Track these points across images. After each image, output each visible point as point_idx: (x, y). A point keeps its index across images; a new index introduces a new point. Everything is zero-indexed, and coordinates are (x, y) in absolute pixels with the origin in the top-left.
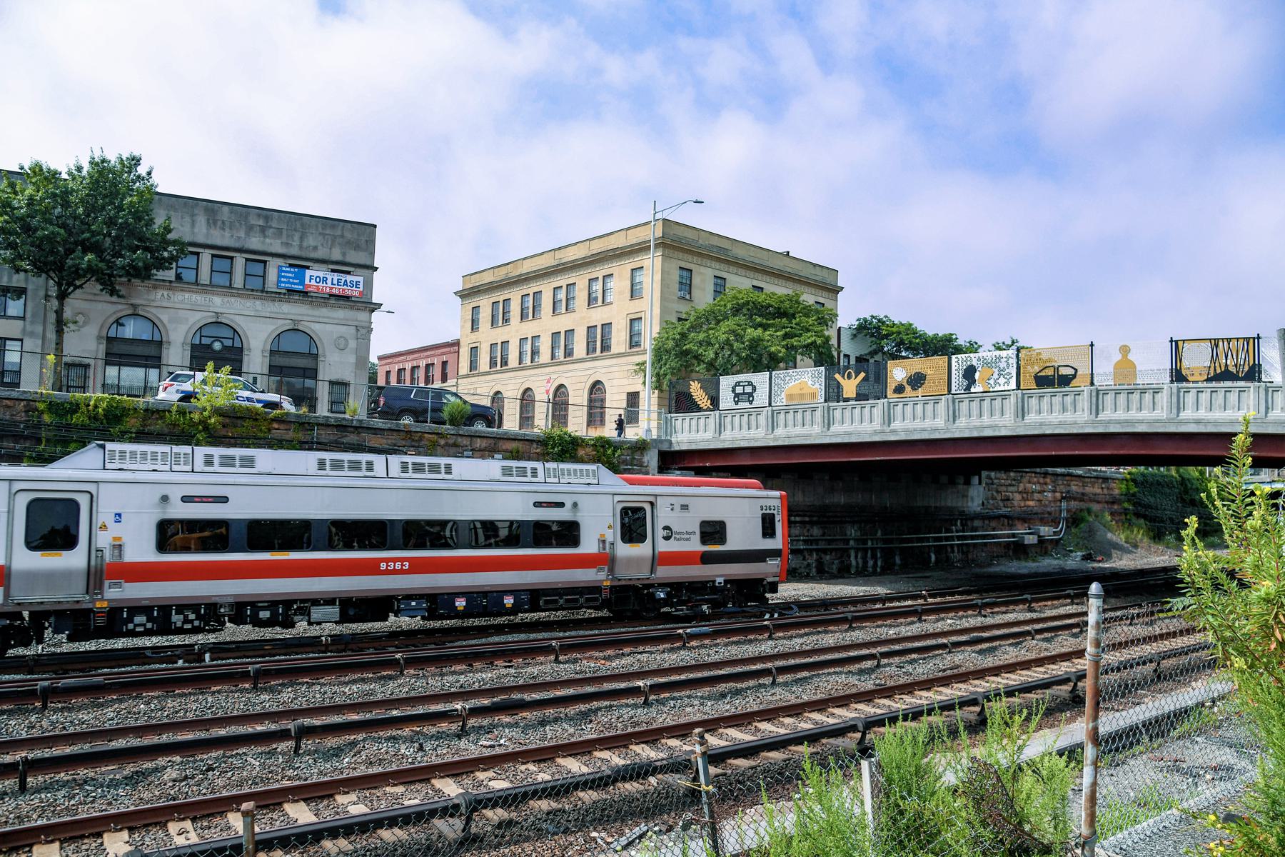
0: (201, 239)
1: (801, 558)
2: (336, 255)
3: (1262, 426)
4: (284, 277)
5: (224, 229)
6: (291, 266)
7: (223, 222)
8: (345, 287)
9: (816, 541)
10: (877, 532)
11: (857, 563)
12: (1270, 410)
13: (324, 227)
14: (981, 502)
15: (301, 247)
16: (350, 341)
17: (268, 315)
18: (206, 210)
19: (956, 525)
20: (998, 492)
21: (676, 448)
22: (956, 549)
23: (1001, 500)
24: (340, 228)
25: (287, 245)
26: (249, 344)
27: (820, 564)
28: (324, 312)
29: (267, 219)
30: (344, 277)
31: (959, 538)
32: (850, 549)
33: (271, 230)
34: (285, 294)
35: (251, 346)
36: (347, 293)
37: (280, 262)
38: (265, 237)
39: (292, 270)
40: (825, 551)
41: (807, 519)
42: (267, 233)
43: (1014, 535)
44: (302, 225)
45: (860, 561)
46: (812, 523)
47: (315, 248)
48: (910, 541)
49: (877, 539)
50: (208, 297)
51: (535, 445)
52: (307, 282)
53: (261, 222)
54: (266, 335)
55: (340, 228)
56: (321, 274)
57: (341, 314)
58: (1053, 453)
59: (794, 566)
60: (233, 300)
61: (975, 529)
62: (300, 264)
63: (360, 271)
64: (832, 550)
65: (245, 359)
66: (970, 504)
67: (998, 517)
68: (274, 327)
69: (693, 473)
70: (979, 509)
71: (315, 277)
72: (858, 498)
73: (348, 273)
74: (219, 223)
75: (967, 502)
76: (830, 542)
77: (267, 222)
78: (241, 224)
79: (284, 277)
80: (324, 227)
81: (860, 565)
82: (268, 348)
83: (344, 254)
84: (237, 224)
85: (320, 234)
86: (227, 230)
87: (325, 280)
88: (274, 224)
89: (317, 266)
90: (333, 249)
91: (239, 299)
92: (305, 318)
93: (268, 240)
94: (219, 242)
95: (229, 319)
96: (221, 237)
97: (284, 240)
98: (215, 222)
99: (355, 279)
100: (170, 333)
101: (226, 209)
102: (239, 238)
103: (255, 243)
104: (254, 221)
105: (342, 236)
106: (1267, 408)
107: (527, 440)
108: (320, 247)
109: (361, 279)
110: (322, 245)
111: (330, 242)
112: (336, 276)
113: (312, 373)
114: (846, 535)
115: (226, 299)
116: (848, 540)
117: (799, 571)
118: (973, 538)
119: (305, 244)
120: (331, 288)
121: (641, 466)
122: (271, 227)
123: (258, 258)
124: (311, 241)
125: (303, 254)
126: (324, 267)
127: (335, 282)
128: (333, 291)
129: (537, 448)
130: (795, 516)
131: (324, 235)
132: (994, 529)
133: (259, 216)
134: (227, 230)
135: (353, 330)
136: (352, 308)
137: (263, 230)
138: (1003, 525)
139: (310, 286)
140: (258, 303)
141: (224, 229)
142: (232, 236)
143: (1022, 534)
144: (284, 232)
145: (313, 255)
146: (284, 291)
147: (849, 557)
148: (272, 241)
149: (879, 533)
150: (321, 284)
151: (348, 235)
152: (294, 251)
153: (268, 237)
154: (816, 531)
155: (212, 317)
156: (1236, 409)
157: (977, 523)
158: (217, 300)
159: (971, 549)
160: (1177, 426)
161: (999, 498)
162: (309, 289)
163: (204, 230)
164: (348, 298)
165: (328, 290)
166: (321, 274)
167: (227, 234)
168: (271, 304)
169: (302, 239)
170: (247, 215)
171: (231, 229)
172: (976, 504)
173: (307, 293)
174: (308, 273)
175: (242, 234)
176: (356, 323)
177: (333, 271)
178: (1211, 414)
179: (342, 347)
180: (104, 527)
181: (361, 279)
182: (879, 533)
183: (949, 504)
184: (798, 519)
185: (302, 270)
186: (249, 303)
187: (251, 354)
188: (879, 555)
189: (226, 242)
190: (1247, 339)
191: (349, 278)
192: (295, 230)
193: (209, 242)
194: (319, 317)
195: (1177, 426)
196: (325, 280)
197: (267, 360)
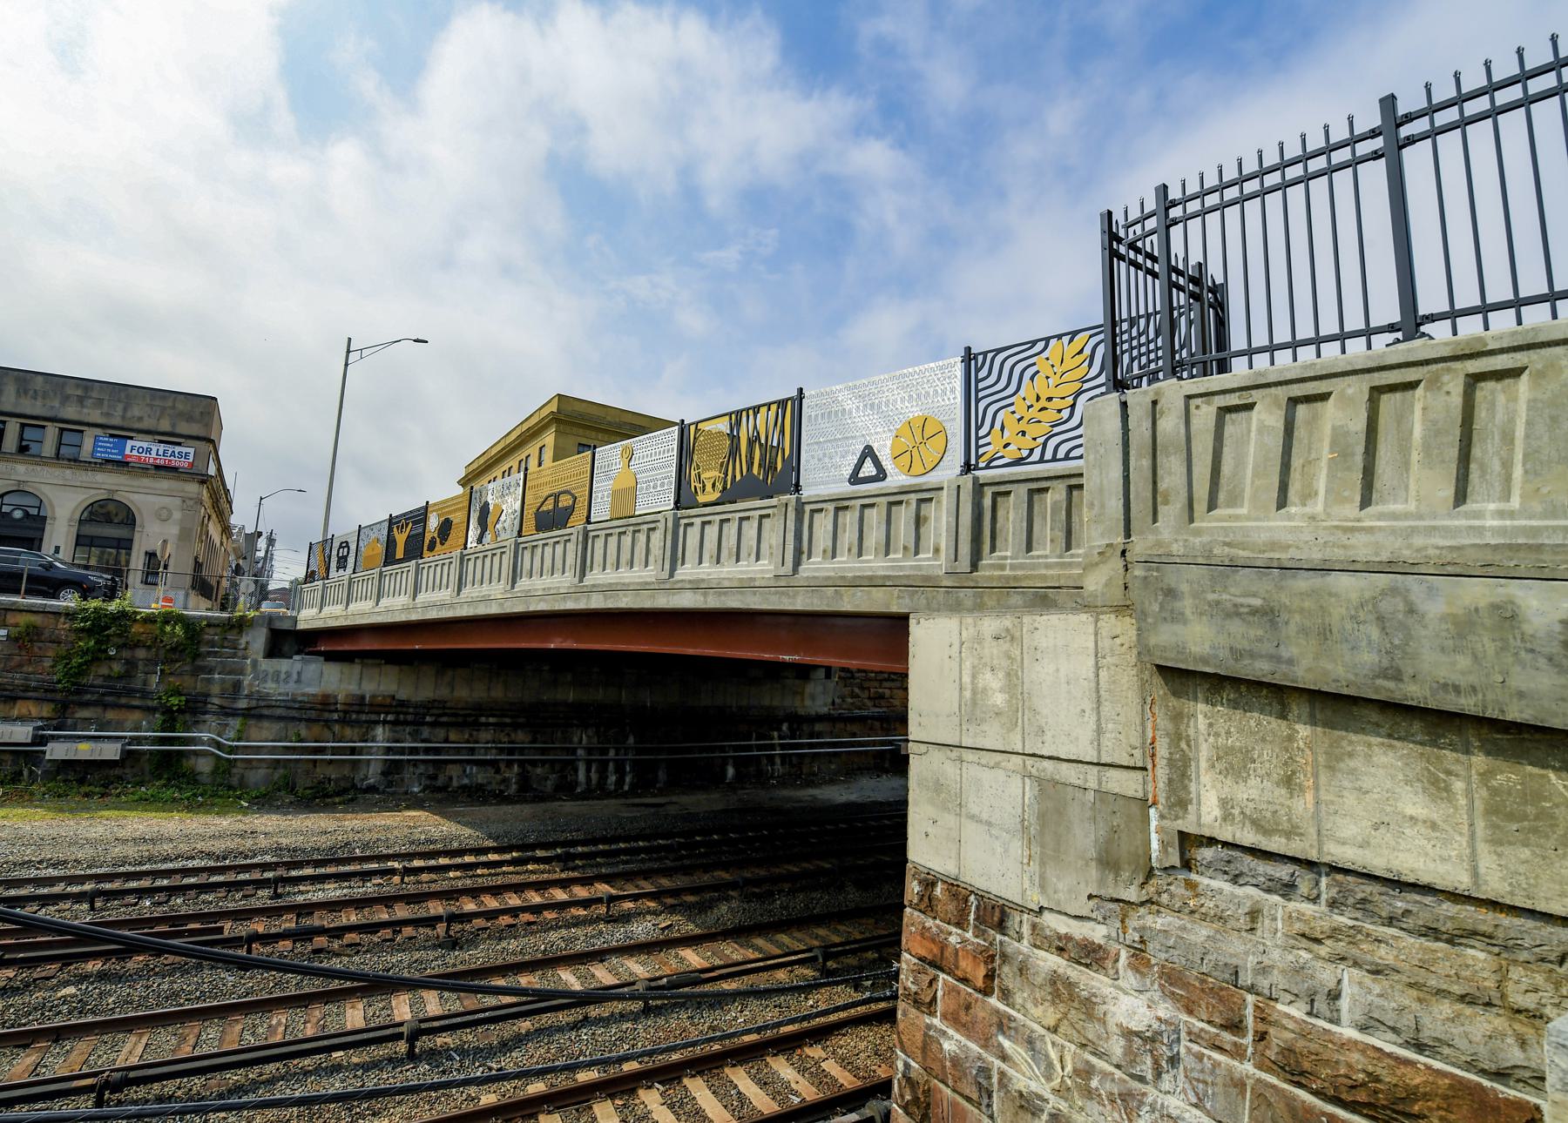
0: (8, 408)
1: (493, 771)
2: (165, 425)
3: (545, 600)
4: (101, 447)
5: (35, 399)
6: (112, 436)
7: (35, 391)
8: (172, 458)
9: (522, 751)
10: (627, 738)
11: (588, 778)
12: (805, 556)
13: (153, 398)
14: (830, 700)
15: (123, 417)
16: (174, 512)
17: (78, 484)
18: (17, 379)
19: (779, 730)
20: (862, 688)
21: (301, 626)
22: (778, 761)
23: (869, 698)
24: (171, 399)
25: (108, 415)
26: (53, 512)
27: (525, 783)
28: (146, 482)
29: (86, 389)
30: (170, 448)
31: (783, 747)
32: (579, 760)
33: (90, 401)
34: (100, 464)
35: (57, 515)
36: (173, 464)
37: (98, 431)
38: (83, 406)
39: (111, 440)
40: (534, 763)
41: (508, 720)
42: (85, 403)
43: (890, 743)
44: (128, 396)
45: (594, 776)
46: (516, 726)
47: (140, 419)
48: (689, 750)
49: (626, 749)
50: (10, 465)
51: (62, 620)
52: (127, 452)
53: (79, 392)
54: (74, 504)
55: (171, 399)
56: (145, 445)
57: (165, 484)
58: (417, 647)
59: (480, 781)
60: (39, 468)
61: (819, 735)
62: (121, 434)
63: (190, 442)
64: (544, 762)
65: (48, 528)
66: (808, 703)
67: (862, 720)
68: (85, 496)
69: (322, 659)
70: (826, 709)
71: (134, 448)
72: (599, 695)
73: (179, 444)
74: (31, 392)
75: (803, 700)
76: (544, 751)
77: (86, 393)
78: (56, 393)
79: (101, 447)
80: (153, 398)
81: (594, 782)
82: (77, 517)
83: (173, 425)
84: (51, 394)
85: (147, 405)
86: (40, 399)
87: (149, 451)
88: (95, 394)
89: (141, 436)
90: (161, 421)
91: (46, 468)
92: (122, 488)
93: (85, 410)
94: (28, 411)
95: (32, 487)
96: (29, 406)
97: (105, 410)
98: (26, 392)
99: (184, 450)
100: (57, 509)
101: (40, 378)
102: (52, 407)
103: (70, 412)
104: (69, 391)
105: (174, 407)
106: (798, 552)
107: (54, 613)
108: (146, 418)
109: (192, 451)
110: (149, 416)
111: (158, 413)
112: (162, 447)
113: (126, 544)
114: (571, 742)
115: (31, 467)
116: (576, 749)
117: (489, 788)
118: (811, 746)
119: (129, 414)
120: (155, 459)
121: (235, 649)
122: (91, 398)
123: (71, 428)
124: (136, 411)
125: (126, 424)
126: (150, 437)
127: (161, 452)
128: (158, 461)
129: (64, 623)
130: (488, 716)
131: (151, 406)
132: (854, 735)
133: (78, 386)
134: (40, 399)
135: (178, 501)
136: (177, 479)
137: (81, 400)
138: (871, 729)
139: (130, 456)
140: (68, 472)
141: (35, 399)
142: (44, 406)
143: (900, 740)
144: (106, 403)
145: (137, 426)
146: (100, 461)
147: (576, 770)
148: (90, 411)
149: (631, 740)
150: (144, 454)
151: (180, 406)
152: (116, 421)
153: (87, 407)
154: (521, 736)
155: (15, 485)
156: (753, 556)
157: (818, 727)
158: (21, 468)
159: (807, 760)
160: (589, 598)
161: (866, 694)
162: (129, 459)
163: (13, 399)
164: (175, 469)
165: (151, 461)
166: (145, 445)
167: (39, 403)
168: (84, 473)
169: (125, 410)
170: (63, 386)
171: (44, 398)
172: (819, 702)
173: (128, 463)
174: (130, 443)
175: (56, 404)
176: (182, 494)
177: (161, 442)
178: (718, 569)
179: (164, 517)
180: (1104, 657)
181: (192, 451)
182: (631, 740)
183: (766, 702)
184: (491, 720)
185: (123, 441)
186: (57, 472)
187: (57, 522)
188: (628, 769)
189: (37, 411)
190: (782, 404)
191: (177, 449)
192: (119, 401)
193: (18, 410)
195: (606, 598)
196: (149, 451)
197: (74, 530)
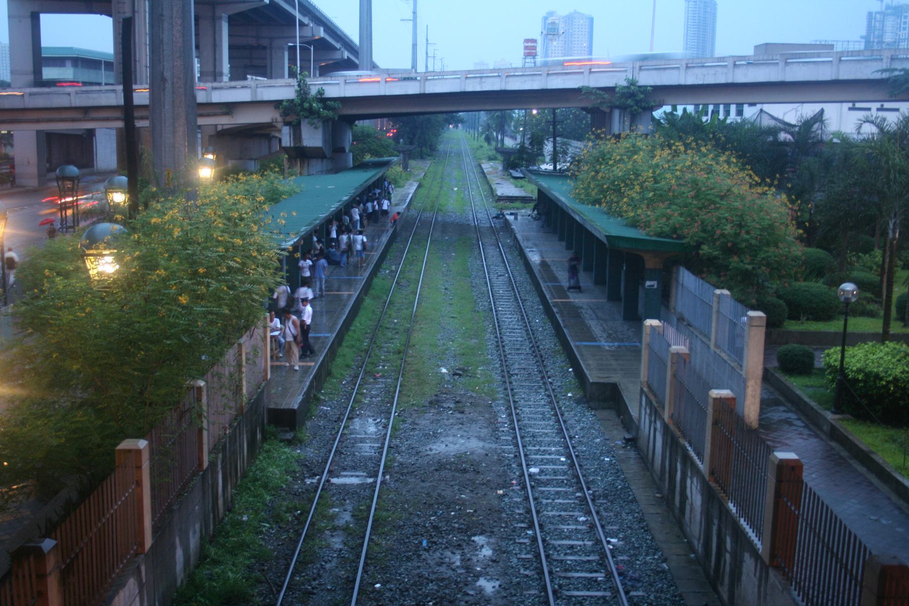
69: (301, 353)
194: (352, 476)
